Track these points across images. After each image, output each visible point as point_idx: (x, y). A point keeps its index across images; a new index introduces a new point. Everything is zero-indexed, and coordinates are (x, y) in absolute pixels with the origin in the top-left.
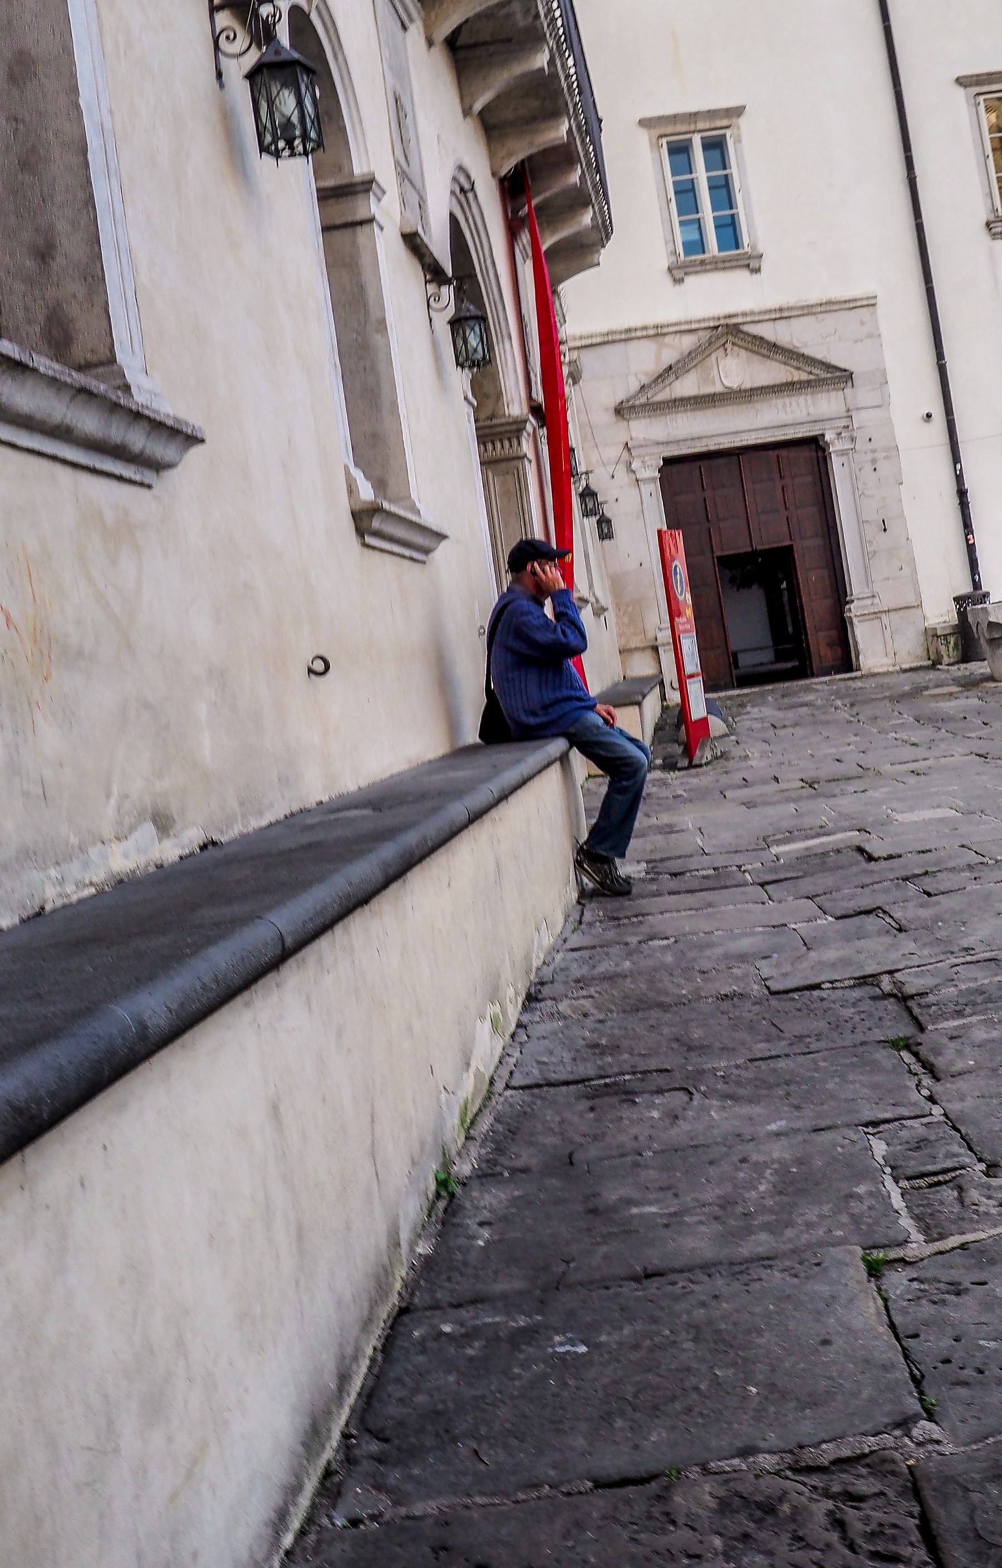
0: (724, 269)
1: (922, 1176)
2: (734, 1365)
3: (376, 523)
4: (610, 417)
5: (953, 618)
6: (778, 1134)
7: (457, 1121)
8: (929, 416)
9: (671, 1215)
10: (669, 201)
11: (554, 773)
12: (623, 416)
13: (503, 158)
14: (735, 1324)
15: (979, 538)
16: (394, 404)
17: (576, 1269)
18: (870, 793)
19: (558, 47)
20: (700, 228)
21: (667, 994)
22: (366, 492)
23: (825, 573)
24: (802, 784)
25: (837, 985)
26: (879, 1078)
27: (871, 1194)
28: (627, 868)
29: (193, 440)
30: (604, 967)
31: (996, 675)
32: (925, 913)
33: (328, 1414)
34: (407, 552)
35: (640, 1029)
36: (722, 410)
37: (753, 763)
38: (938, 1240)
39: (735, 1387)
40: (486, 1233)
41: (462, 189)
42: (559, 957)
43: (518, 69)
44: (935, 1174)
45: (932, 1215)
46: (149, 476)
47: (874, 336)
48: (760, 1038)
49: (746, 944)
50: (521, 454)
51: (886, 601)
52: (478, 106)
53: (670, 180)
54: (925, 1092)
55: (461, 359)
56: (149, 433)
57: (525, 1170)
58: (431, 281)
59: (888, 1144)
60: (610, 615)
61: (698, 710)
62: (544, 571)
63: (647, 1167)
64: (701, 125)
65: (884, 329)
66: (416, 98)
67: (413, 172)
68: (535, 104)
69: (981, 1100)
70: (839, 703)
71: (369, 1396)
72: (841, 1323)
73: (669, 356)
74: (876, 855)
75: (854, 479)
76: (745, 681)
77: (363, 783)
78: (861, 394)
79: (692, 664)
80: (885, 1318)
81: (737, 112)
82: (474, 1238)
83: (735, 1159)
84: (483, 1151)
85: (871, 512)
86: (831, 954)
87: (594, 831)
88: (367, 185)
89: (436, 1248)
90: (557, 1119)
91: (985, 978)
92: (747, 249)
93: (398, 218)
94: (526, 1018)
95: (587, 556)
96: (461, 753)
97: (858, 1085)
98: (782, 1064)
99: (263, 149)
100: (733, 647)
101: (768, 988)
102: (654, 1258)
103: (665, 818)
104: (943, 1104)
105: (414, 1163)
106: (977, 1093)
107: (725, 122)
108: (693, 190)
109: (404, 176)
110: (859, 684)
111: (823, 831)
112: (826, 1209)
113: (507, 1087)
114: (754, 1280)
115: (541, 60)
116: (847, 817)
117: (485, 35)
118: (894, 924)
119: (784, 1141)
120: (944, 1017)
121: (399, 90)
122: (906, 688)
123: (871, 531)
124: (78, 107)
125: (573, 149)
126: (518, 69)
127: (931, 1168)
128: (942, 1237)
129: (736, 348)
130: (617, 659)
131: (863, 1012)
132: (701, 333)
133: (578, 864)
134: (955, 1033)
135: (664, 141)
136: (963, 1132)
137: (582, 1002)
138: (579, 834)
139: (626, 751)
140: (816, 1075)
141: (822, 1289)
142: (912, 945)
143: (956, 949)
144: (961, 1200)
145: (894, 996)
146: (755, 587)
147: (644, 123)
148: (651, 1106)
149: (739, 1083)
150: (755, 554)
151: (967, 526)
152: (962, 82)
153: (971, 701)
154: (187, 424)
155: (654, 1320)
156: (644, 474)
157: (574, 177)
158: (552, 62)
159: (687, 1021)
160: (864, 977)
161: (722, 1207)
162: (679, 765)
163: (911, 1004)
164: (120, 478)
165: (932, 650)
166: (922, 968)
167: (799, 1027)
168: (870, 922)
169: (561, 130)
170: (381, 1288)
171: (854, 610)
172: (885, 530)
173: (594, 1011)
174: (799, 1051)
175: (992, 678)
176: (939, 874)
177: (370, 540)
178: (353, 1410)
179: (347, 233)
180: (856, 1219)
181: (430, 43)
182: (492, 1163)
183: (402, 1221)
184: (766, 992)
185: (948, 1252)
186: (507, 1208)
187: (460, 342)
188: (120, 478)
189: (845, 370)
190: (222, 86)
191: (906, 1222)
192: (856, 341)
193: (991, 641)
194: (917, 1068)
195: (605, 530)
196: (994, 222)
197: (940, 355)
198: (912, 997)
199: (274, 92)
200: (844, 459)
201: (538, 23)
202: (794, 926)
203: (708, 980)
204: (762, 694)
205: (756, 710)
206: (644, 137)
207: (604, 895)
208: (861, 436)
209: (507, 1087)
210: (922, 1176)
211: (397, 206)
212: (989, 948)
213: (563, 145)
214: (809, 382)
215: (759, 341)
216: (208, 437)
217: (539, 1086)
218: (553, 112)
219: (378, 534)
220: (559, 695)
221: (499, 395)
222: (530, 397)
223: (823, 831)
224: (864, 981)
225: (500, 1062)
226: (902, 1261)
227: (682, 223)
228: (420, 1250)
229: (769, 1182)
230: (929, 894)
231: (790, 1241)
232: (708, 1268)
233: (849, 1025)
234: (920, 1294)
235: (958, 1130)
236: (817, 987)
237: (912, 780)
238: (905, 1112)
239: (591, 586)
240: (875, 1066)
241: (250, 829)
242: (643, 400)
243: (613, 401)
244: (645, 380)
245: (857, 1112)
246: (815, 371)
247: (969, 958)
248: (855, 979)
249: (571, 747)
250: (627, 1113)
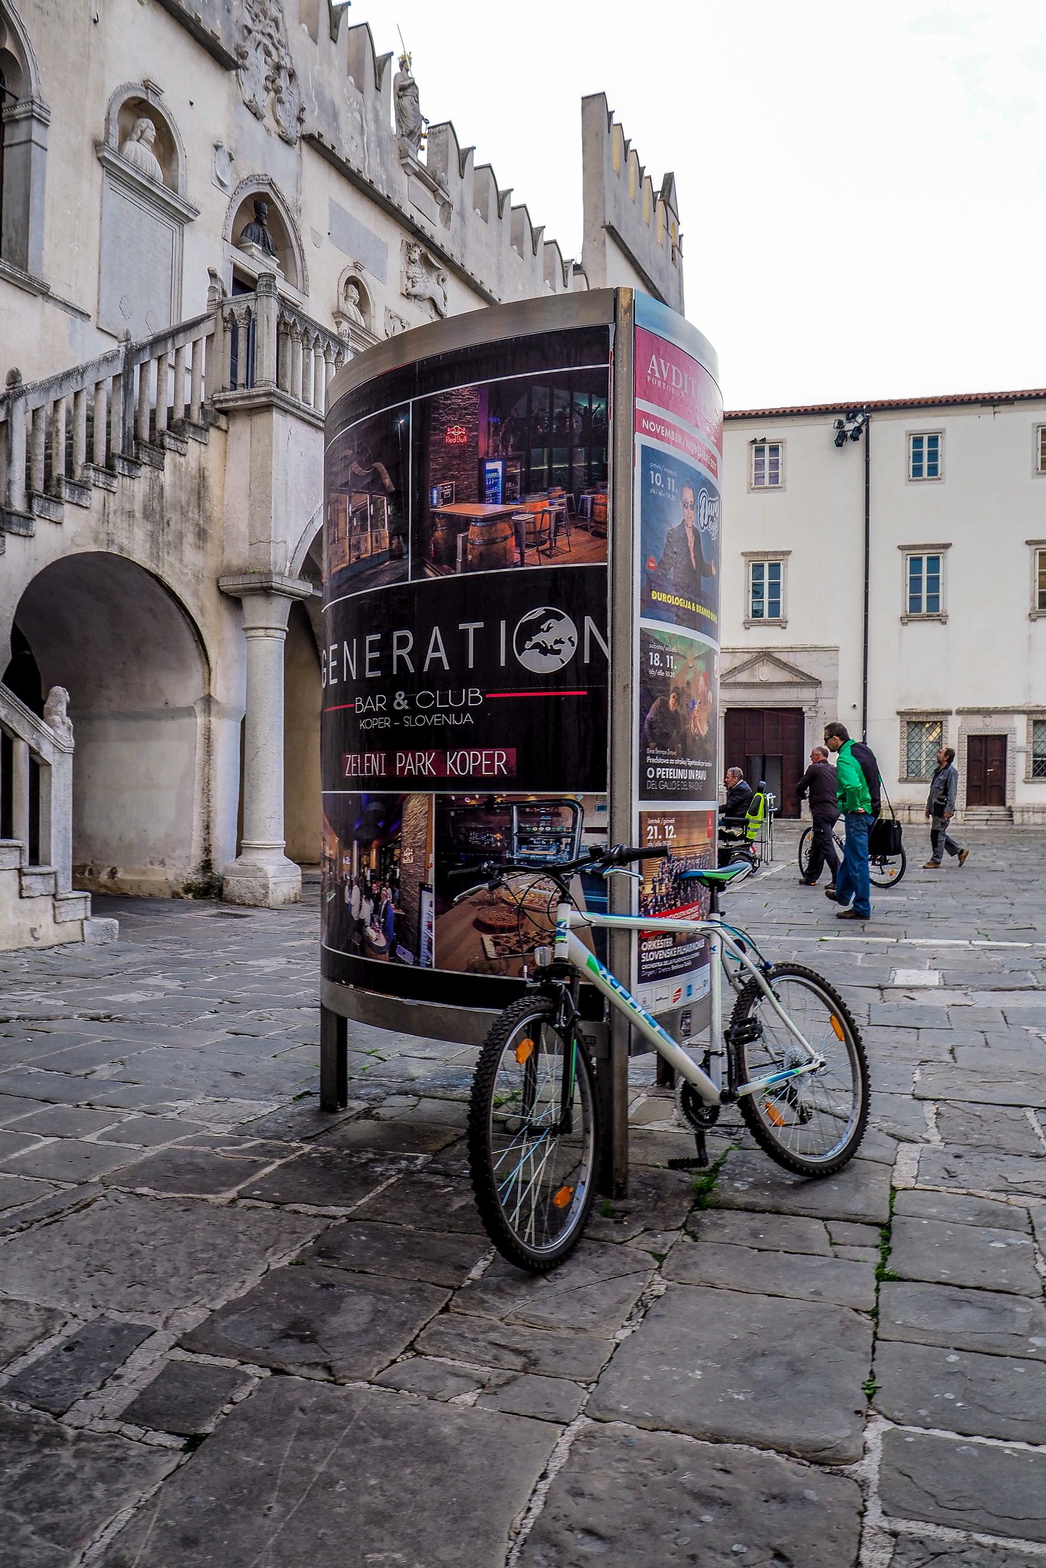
73: (737, 663)
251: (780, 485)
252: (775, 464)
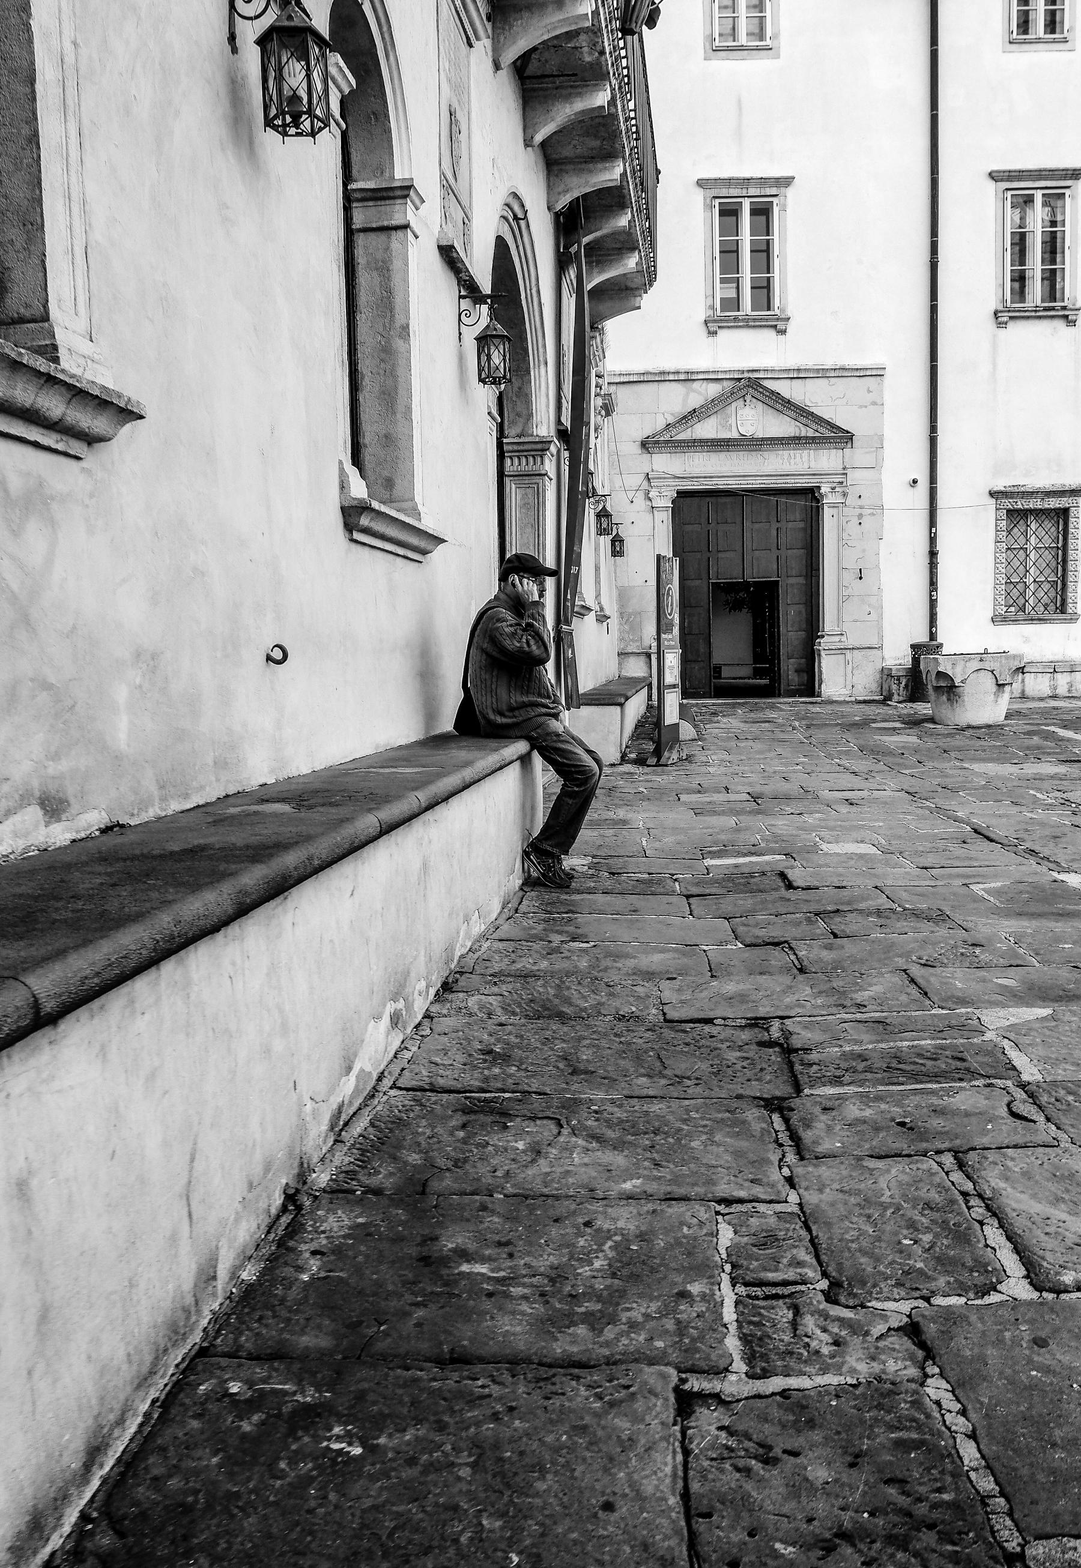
0: (754, 327)
1: (761, 1284)
2: (503, 1515)
3: (365, 521)
4: (636, 449)
5: (908, 662)
6: (630, 1197)
7: (324, 1127)
8: (915, 482)
9: (498, 1280)
10: (713, 259)
11: (512, 776)
12: (647, 449)
13: (559, 194)
14: (522, 1453)
15: (942, 596)
16: (409, 409)
17: (386, 1334)
18: (806, 818)
19: (620, 88)
20: (738, 288)
21: (571, 1004)
22: (359, 489)
23: (802, 608)
24: (750, 798)
25: (729, 1022)
26: (744, 1144)
27: (704, 1297)
28: (573, 862)
29: (128, 414)
30: (525, 964)
31: (937, 719)
32: (827, 956)
33: (62, 1499)
34: (401, 551)
35: (534, 1042)
36: (734, 455)
37: (711, 770)
38: (759, 1378)
39: (496, 1550)
40: (314, 1264)
41: (516, 218)
42: (486, 945)
43: (580, 105)
44: (775, 1284)
45: (761, 1339)
46: (76, 447)
47: (878, 404)
48: (642, 1071)
49: (655, 960)
50: (543, 472)
51: (851, 641)
52: (539, 138)
53: (717, 239)
54: (786, 1172)
55: (483, 376)
56: (69, 402)
57: (378, 1192)
58: (464, 297)
59: (736, 1232)
60: (614, 622)
61: (671, 715)
62: (521, 584)
63: (493, 1212)
64: (752, 191)
65: (888, 398)
66: (473, 115)
67: (461, 187)
68: (596, 143)
69: (840, 1196)
70: (797, 724)
71: (129, 1463)
72: (632, 1484)
73: (695, 401)
74: (795, 884)
75: (841, 529)
76: (722, 692)
77: (319, 766)
78: (856, 455)
79: (672, 674)
80: (680, 1484)
81: (786, 182)
82: (300, 1269)
83: (581, 1220)
84: (347, 1159)
85: (851, 560)
86: (730, 987)
87: (546, 828)
88: (405, 191)
89: (263, 1273)
90: (428, 1132)
91: (871, 1042)
92: (777, 312)
93: (436, 229)
94: (435, 1009)
95: (597, 569)
96: (436, 741)
97: (722, 1149)
98: (656, 1107)
99: (269, 123)
100: (716, 659)
101: (664, 1014)
102: (465, 1336)
103: (621, 813)
104: (801, 1191)
105: (251, 1186)
106: (836, 1186)
107: (774, 191)
108: (737, 251)
109: (449, 189)
110: (817, 709)
111: (754, 850)
112: (654, 1306)
113: (394, 1086)
114: (556, 1394)
115: (601, 98)
116: (777, 838)
117: (552, 67)
118: (796, 962)
119: (632, 1208)
120: (822, 1081)
121: (455, 105)
122: (857, 718)
123: (849, 577)
124: (28, 28)
125: (626, 192)
126: (580, 105)
127: (771, 1276)
128: (765, 1375)
129: (754, 400)
130: (615, 659)
131: (748, 1058)
132: (726, 383)
133: (526, 854)
134: (829, 1104)
135: (718, 201)
136: (814, 1233)
137: (491, 999)
138: (532, 827)
139: (580, 760)
140: (686, 1127)
141: (622, 1424)
142: (808, 991)
143: (848, 1003)
144: (794, 1325)
145: (781, 1045)
146: (745, 611)
147: (701, 183)
148: (519, 1135)
149: (609, 1124)
150: (746, 584)
151: (933, 584)
152: (992, 494)
153: (910, 739)
154: (120, 396)
155: (441, 1427)
156: (659, 502)
157: (623, 221)
158: (612, 102)
159: (581, 1039)
160: (756, 1019)
161: (552, 1280)
162: (648, 762)
163: (794, 1057)
164: (36, 445)
165: (885, 687)
166: (812, 1019)
167: (680, 1066)
168: (778, 958)
169: (613, 173)
170: (176, 1332)
171: (824, 644)
172: (861, 578)
173: (499, 1012)
174: (676, 1095)
175: (932, 720)
176: (849, 915)
177: (357, 536)
178: (105, 1481)
179: (382, 237)
180: (681, 1328)
181: (497, 66)
182: (350, 1174)
183: (223, 1252)
184: (662, 1018)
185: (766, 1397)
186: (344, 1237)
187: (484, 358)
188: (36, 445)
189: (848, 432)
190: (235, 50)
191: (732, 1344)
192: (861, 407)
193: (937, 689)
194: (784, 1137)
195: (617, 548)
196: (1001, 312)
197: (933, 429)
198: (796, 1050)
199: (284, 59)
200: (834, 511)
201: (603, 58)
202: (705, 948)
203: (612, 994)
204: (734, 706)
205: (725, 720)
206: (699, 197)
207: (545, 885)
208: (850, 490)
209: (394, 1086)
210: (761, 1284)
211: (436, 218)
212: (879, 1009)
213: (616, 187)
214: (814, 438)
215: (775, 396)
216: (149, 411)
217: (422, 1090)
218: (610, 154)
219: (366, 531)
220: (525, 699)
221: (530, 416)
222: (559, 422)
223: (754, 850)
224: (756, 1023)
225: (395, 1057)
226: (717, 1397)
227: (723, 281)
228: (245, 1276)
229: (606, 1257)
230: (835, 936)
231: (607, 1344)
232: (515, 1362)
233: (730, 1071)
234: (726, 1454)
235: (809, 1229)
236: (709, 1021)
237: (844, 809)
238: (758, 1191)
239: (598, 596)
240: (740, 1128)
241: (170, 812)
242: (667, 437)
243: (640, 436)
244: (671, 420)
245: (714, 1184)
246: (821, 430)
247: (859, 1016)
248: (748, 1019)
249: (532, 749)
250: (496, 1139)
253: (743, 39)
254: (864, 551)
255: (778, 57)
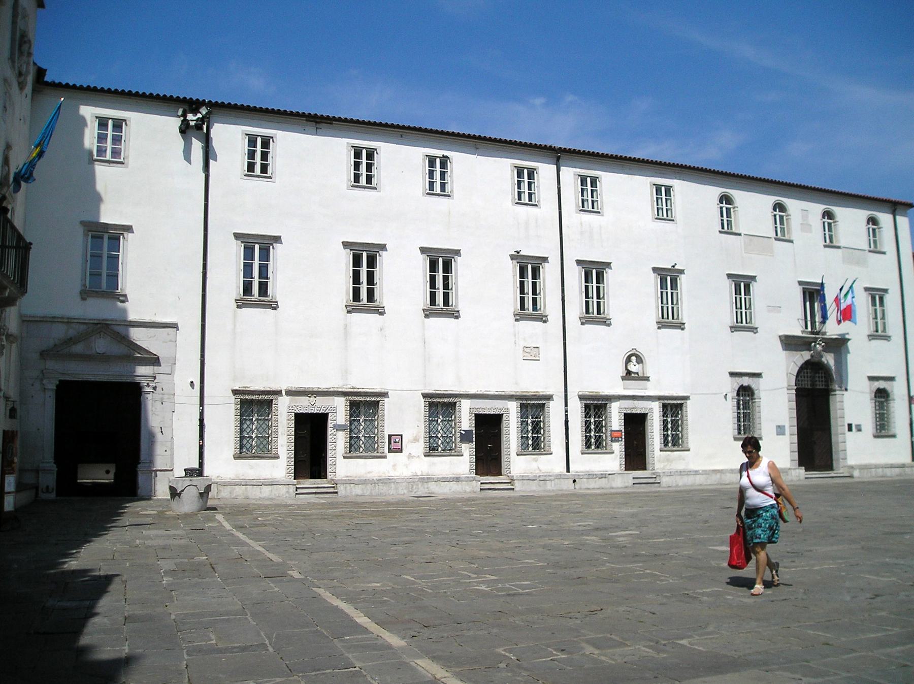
73: (72, 333)
251: (122, 160)
252: (117, 140)
253: (880, 333)
254: (164, 418)
255: (127, 167)
